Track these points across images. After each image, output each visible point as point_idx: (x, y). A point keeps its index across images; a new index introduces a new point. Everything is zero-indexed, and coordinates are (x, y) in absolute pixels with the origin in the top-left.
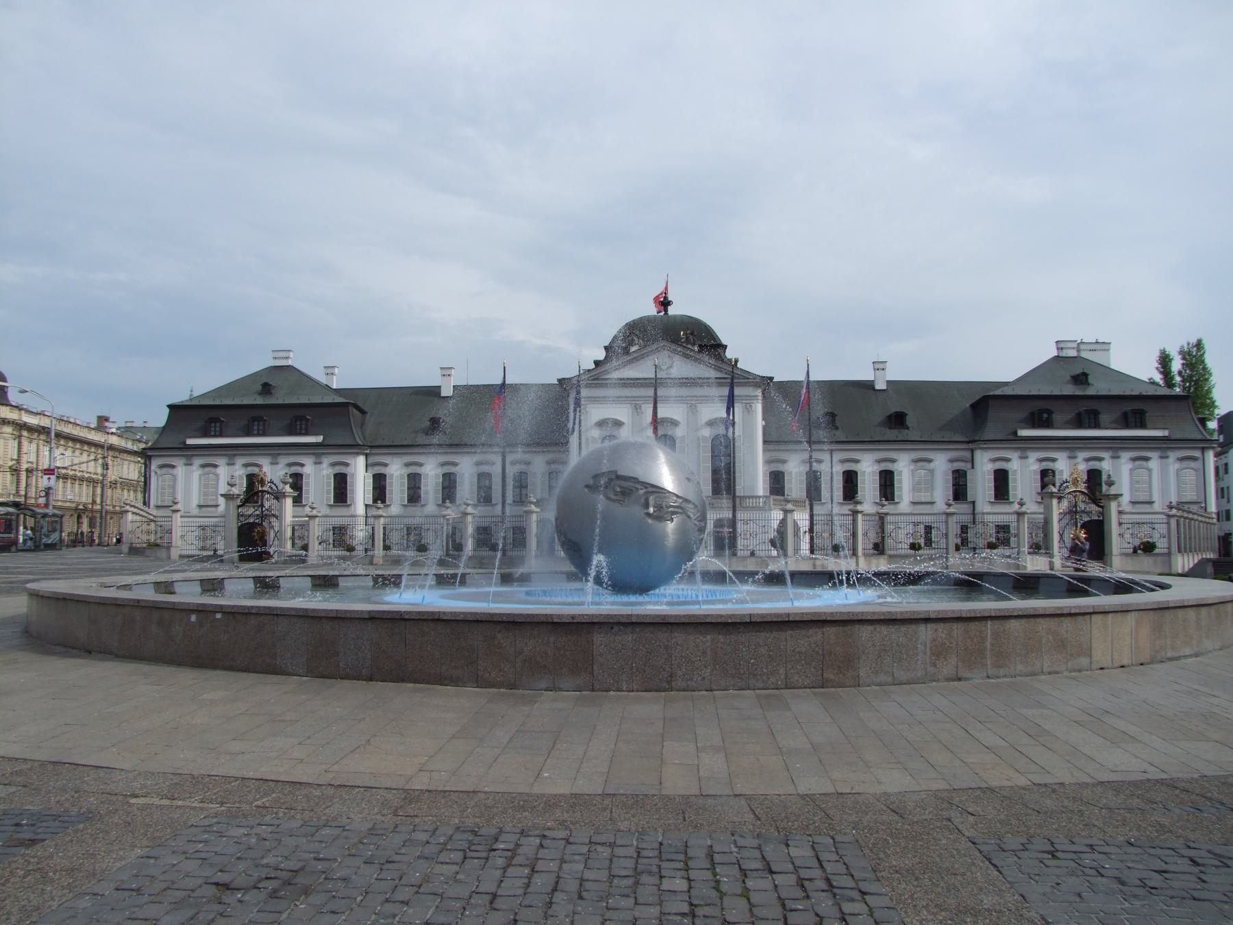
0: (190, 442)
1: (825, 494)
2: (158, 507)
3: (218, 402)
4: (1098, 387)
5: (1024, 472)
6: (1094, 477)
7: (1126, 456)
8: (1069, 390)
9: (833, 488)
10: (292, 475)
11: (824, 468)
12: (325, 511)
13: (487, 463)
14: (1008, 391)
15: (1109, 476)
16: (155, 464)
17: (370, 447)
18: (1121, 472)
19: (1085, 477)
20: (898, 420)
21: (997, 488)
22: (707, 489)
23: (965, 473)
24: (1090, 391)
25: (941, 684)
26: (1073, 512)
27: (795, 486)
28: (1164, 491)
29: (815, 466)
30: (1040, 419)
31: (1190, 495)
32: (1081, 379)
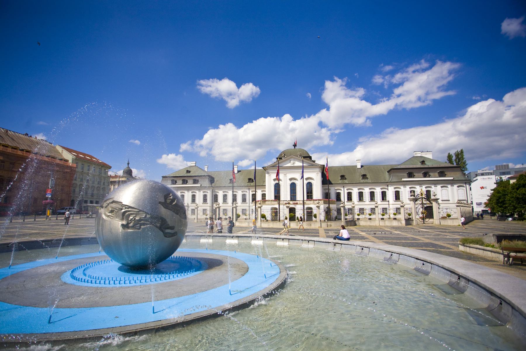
0: (403, 180)
1: (342, 199)
2: (442, 201)
3: (439, 166)
4: (428, 164)
5: (405, 191)
6: (428, 192)
7: (439, 187)
8: (419, 165)
9: (249, 198)
10: (411, 191)
11: (247, 194)
12: (357, 203)
13: (245, 191)
14: (399, 167)
15: (434, 193)
16: (345, 189)
17: (377, 183)
18: (437, 191)
19: (425, 193)
20: (364, 176)
21: (396, 197)
22: (273, 198)
23: (385, 192)
24: (425, 166)
25: (16, 240)
26: (422, 204)
27: (333, 197)
28: (453, 197)
29: (234, 193)
30: (410, 175)
31: (464, 198)
32: (423, 162)
